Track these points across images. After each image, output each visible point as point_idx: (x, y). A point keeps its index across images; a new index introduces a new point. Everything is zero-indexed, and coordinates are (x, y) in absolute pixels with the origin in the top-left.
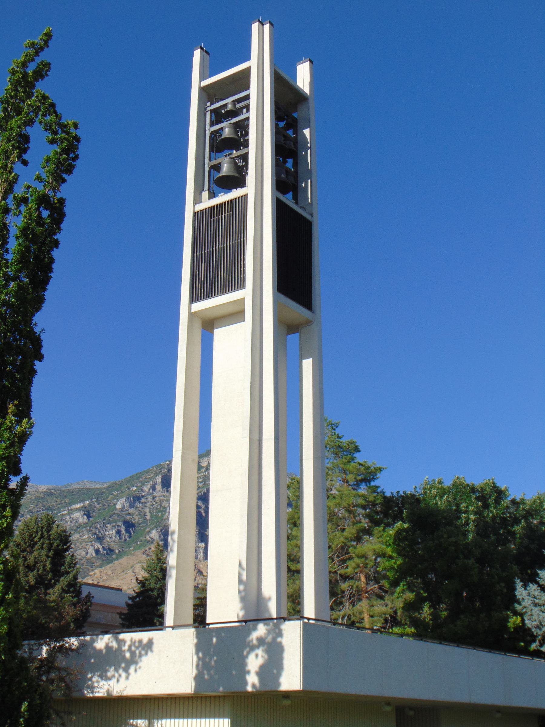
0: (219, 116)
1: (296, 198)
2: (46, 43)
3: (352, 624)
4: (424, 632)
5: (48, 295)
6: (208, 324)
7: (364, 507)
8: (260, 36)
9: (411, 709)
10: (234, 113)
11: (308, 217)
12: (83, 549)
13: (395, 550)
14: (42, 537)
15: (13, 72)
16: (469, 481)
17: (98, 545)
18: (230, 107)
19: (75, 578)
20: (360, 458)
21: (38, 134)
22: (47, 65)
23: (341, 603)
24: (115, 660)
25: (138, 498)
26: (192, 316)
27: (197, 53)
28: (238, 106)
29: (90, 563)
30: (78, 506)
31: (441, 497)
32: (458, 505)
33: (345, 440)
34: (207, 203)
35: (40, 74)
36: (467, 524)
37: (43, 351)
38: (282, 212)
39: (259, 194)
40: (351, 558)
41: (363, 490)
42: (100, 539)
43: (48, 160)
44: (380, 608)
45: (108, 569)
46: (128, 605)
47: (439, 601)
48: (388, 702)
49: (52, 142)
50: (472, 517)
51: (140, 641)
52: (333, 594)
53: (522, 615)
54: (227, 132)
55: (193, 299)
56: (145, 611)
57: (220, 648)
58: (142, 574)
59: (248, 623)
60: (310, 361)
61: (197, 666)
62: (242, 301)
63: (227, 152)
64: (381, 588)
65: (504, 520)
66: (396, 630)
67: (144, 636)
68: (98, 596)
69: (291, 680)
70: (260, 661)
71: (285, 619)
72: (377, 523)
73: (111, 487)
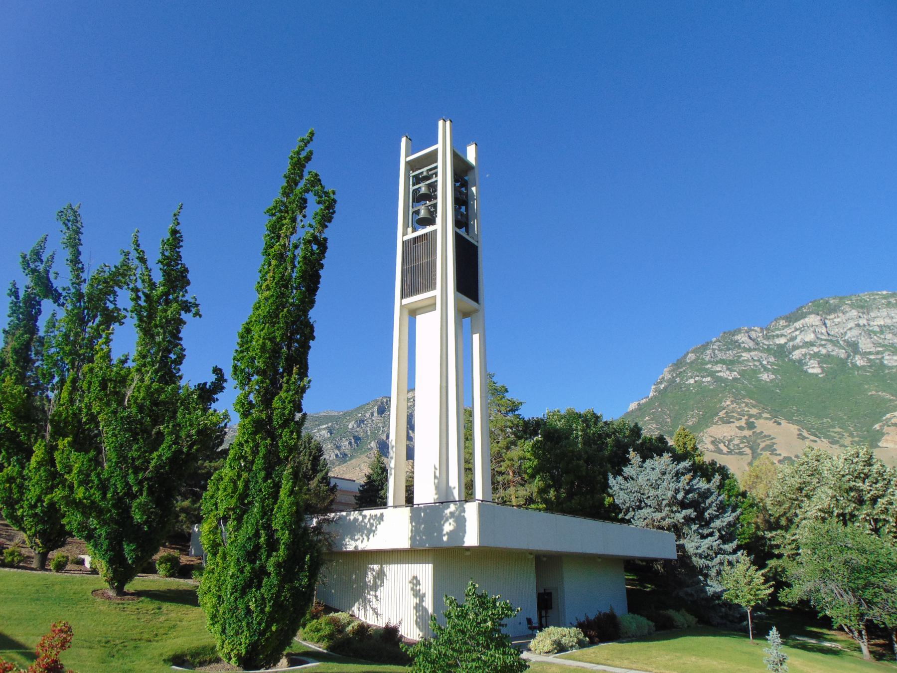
0: (418, 180)
1: (467, 231)
2: (311, 139)
3: (504, 503)
4: (553, 507)
5: (317, 298)
6: (413, 313)
7: (511, 428)
8: (444, 129)
9: (544, 556)
10: (427, 178)
11: (476, 243)
12: (329, 455)
13: (533, 455)
14: (305, 447)
15: (292, 158)
16: (577, 410)
17: (337, 452)
18: (425, 174)
19: (327, 473)
20: (508, 396)
21: (311, 198)
22: (311, 153)
23: (497, 489)
24: (355, 529)
25: (362, 421)
26: (402, 307)
27: (404, 140)
28: (430, 173)
29: (333, 463)
30: (324, 426)
31: (560, 421)
32: (570, 426)
33: (499, 385)
34: (411, 235)
35: (308, 158)
36: (577, 437)
37: (315, 334)
38: (459, 241)
39: (444, 229)
40: (504, 461)
41: (510, 417)
42: (338, 448)
43: (316, 214)
44: (523, 492)
45: (343, 467)
46: (360, 490)
47: (560, 487)
48: (531, 552)
49: (319, 203)
50: (580, 433)
51: (376, 516)
52: (493, 483)
53: (612, 496)
54: (423, 190)
55: (403, 296)
56: (372, 495)
57: (426, 519)
58: (368, 471)
59: (444, 502)
60: (478, 335)
61: (412, 531)
62: (435, 297)
63: (423, 202)
64: (522, 479)
65: (600, 435)
66: (533, 506)
67: (377, 512)
68: (341, 485)
69: (471, 539)
70: (451, 528)
71: (466, 501)
72: (520, 438)
73: (345, 415)
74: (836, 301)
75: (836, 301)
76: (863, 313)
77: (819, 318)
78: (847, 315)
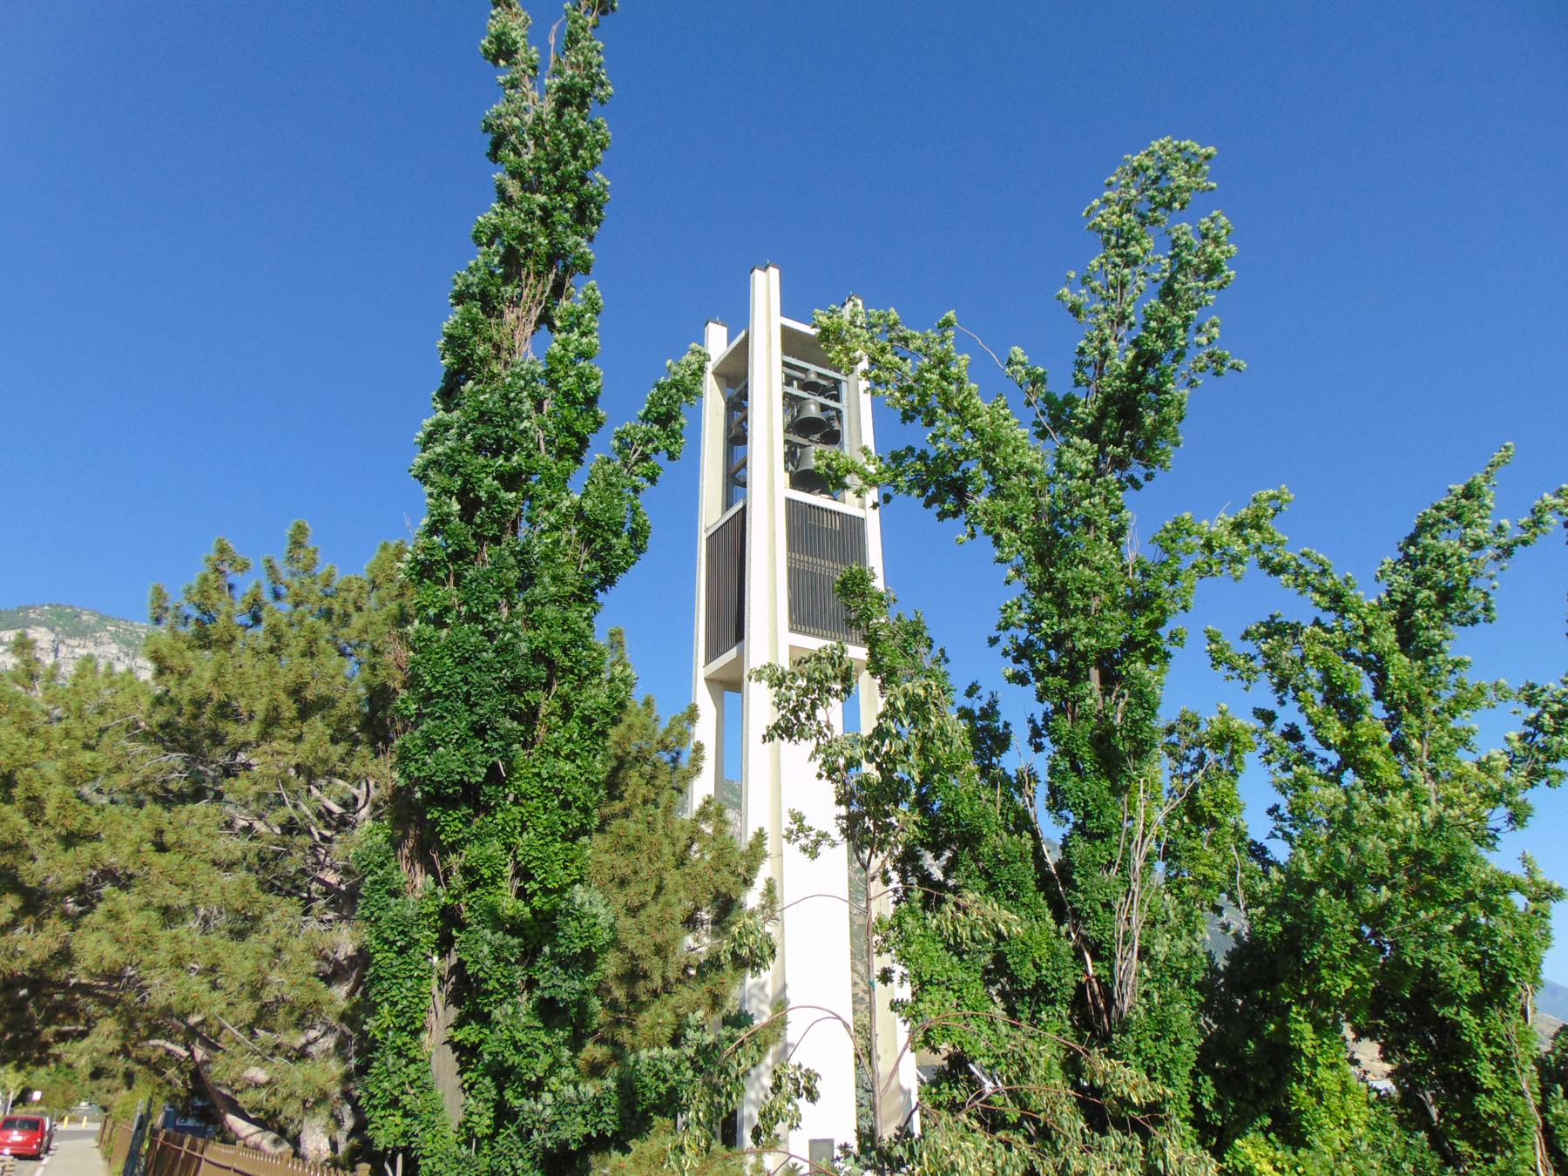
60: (774, 273)
74: (93, 620)
75: (93, 620)
76: (127, 654)
77: (52, 636)
78: (101, 648)
